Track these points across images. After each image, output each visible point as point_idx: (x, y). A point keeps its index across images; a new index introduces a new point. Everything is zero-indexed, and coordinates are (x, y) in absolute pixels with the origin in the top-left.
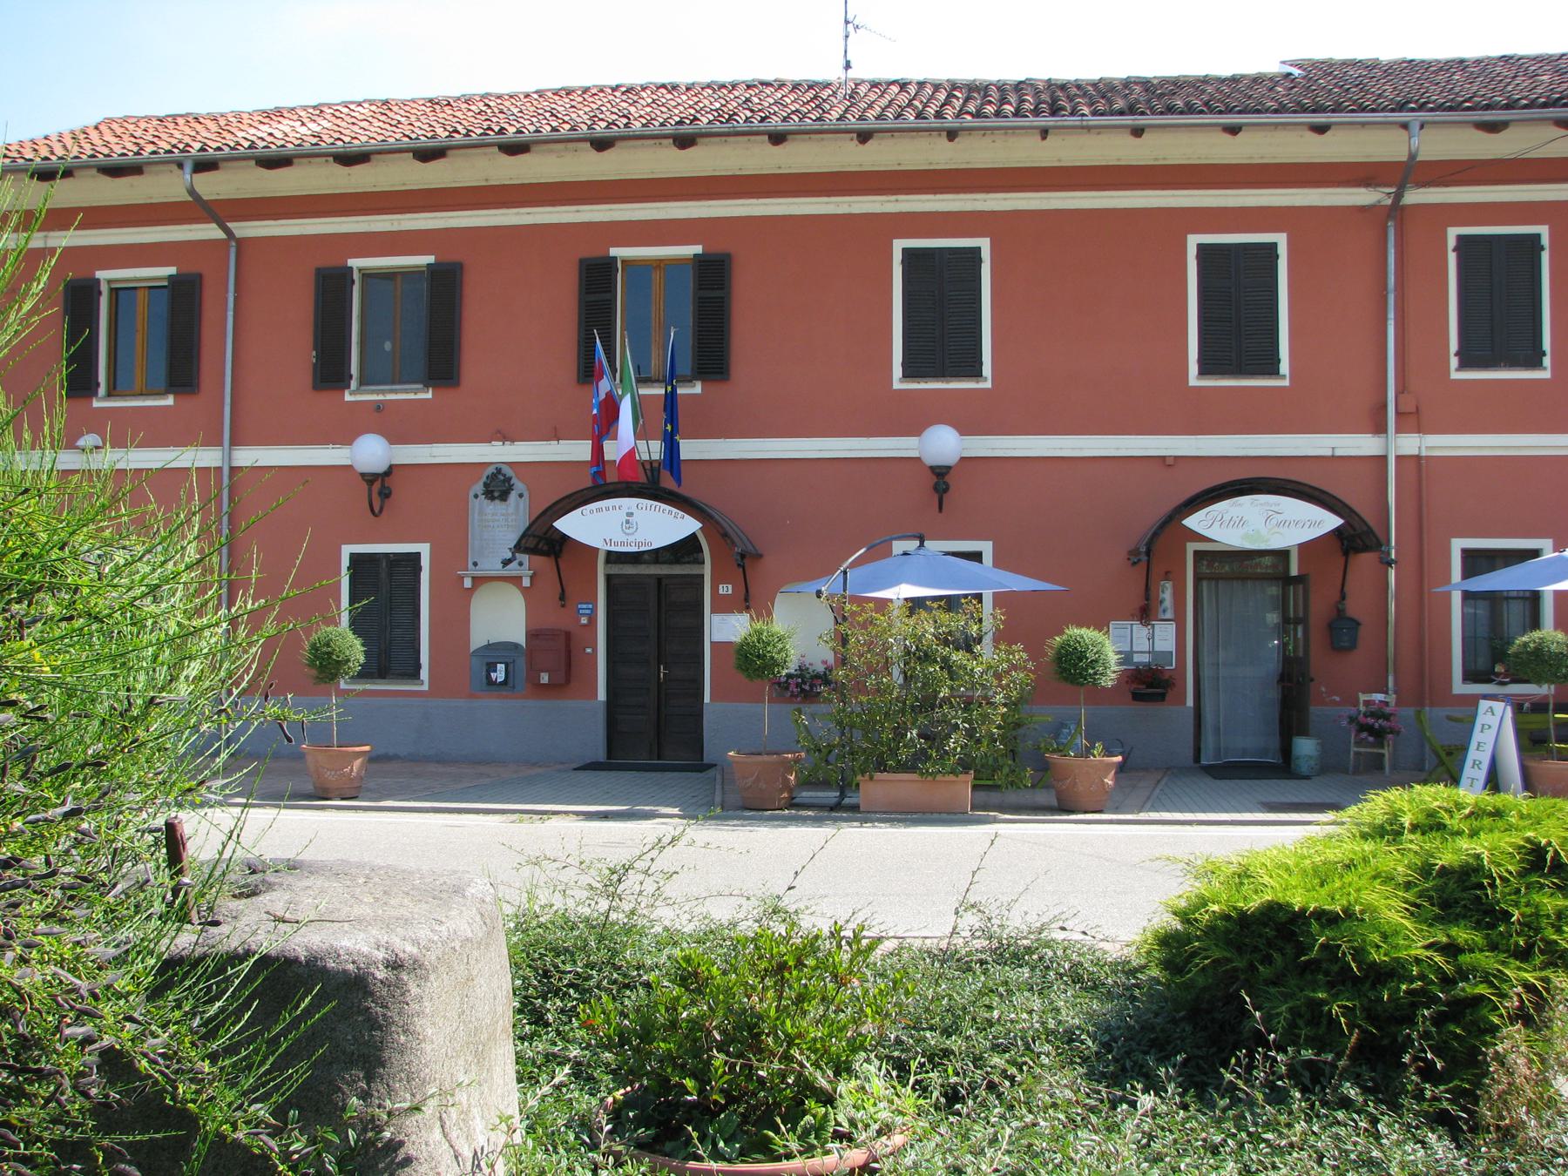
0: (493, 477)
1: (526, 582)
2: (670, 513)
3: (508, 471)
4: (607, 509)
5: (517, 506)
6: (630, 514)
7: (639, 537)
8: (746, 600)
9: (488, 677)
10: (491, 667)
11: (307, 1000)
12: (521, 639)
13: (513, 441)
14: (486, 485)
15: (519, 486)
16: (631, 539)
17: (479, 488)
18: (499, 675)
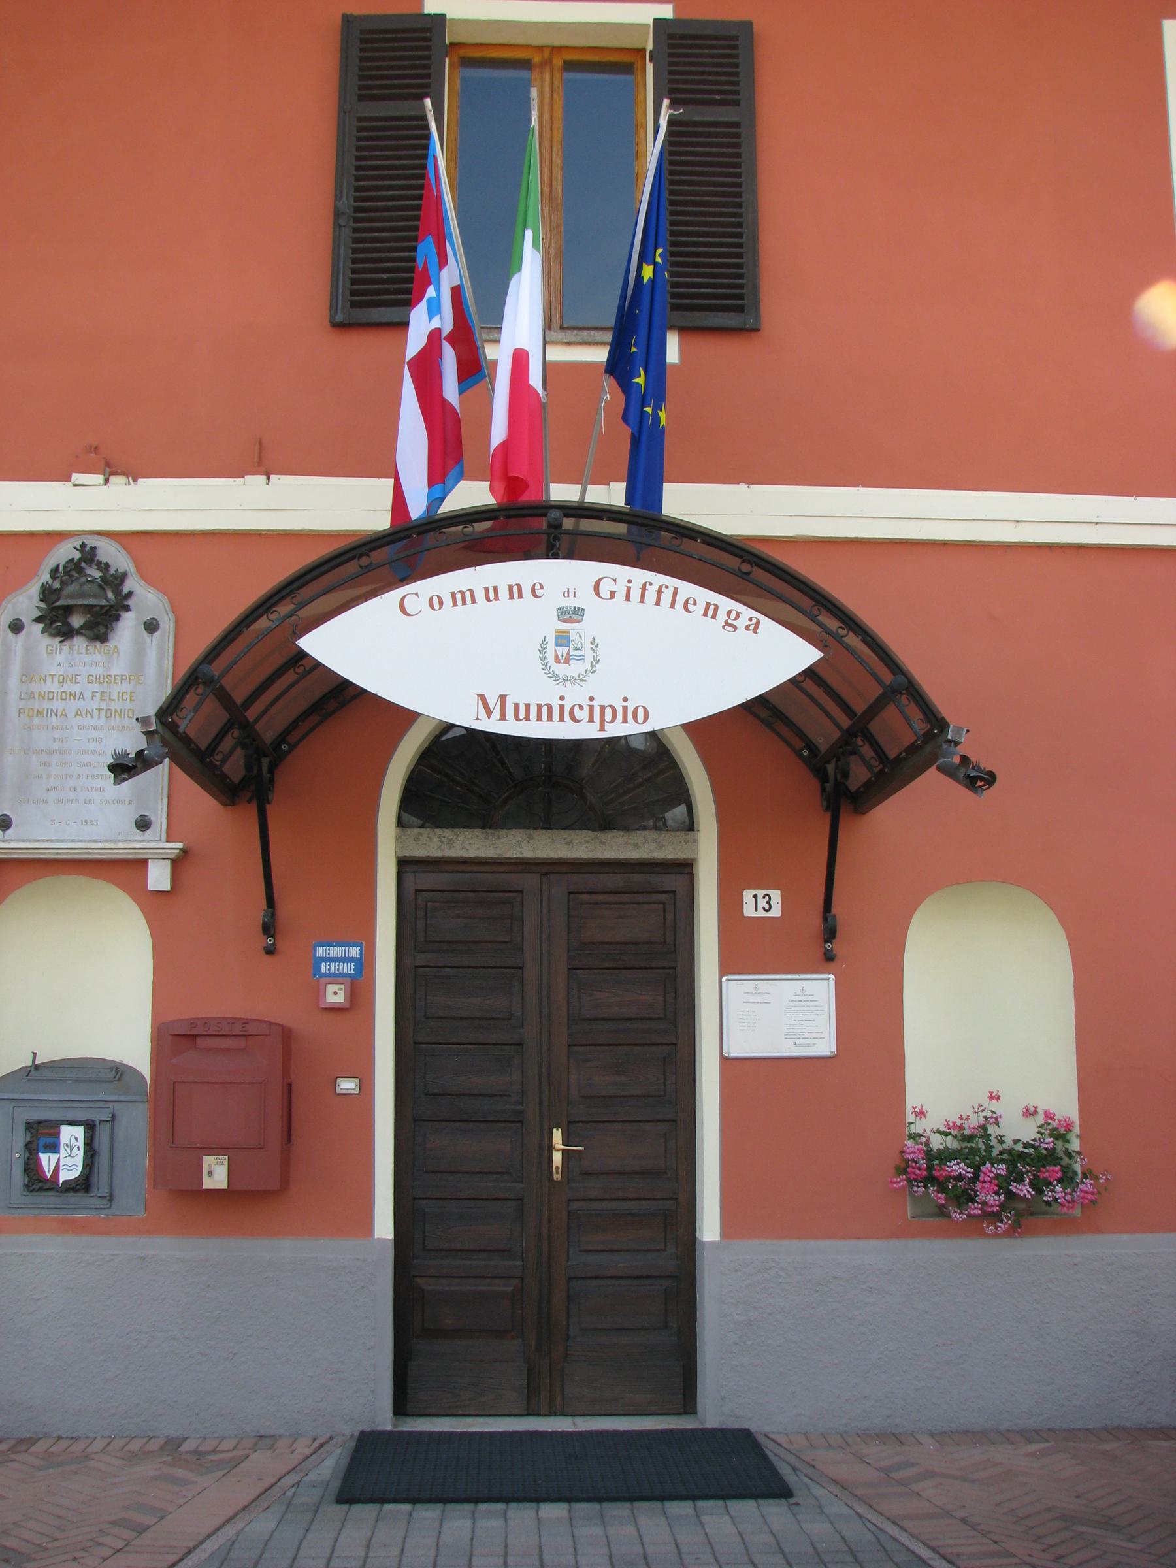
0: (73, 569)
1: (159, 877)
2: (710, 611)
3: (116, 557)
4: (492, 595)
5: (139, 654)
6: (572, 615)
7: (606, 689)
8: (830, 933)
9: (32, 1168)
10: (42, 1135)
11: (534, 122)
12: (134, 1048)
13: (134, 474)
14: (47, 593)
15: (146, 598)
16: (576, 696)
17: (26, 602)
18: (67, 1159)
